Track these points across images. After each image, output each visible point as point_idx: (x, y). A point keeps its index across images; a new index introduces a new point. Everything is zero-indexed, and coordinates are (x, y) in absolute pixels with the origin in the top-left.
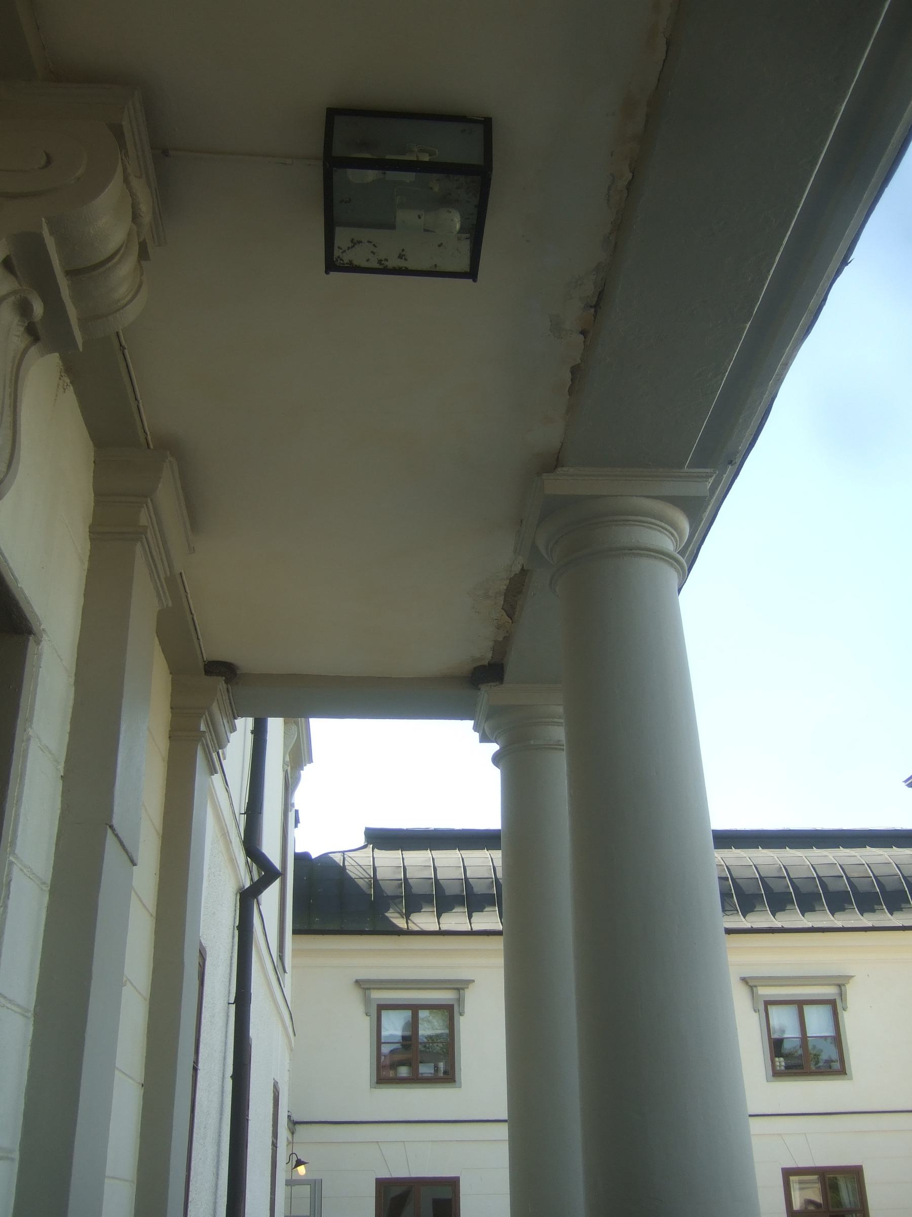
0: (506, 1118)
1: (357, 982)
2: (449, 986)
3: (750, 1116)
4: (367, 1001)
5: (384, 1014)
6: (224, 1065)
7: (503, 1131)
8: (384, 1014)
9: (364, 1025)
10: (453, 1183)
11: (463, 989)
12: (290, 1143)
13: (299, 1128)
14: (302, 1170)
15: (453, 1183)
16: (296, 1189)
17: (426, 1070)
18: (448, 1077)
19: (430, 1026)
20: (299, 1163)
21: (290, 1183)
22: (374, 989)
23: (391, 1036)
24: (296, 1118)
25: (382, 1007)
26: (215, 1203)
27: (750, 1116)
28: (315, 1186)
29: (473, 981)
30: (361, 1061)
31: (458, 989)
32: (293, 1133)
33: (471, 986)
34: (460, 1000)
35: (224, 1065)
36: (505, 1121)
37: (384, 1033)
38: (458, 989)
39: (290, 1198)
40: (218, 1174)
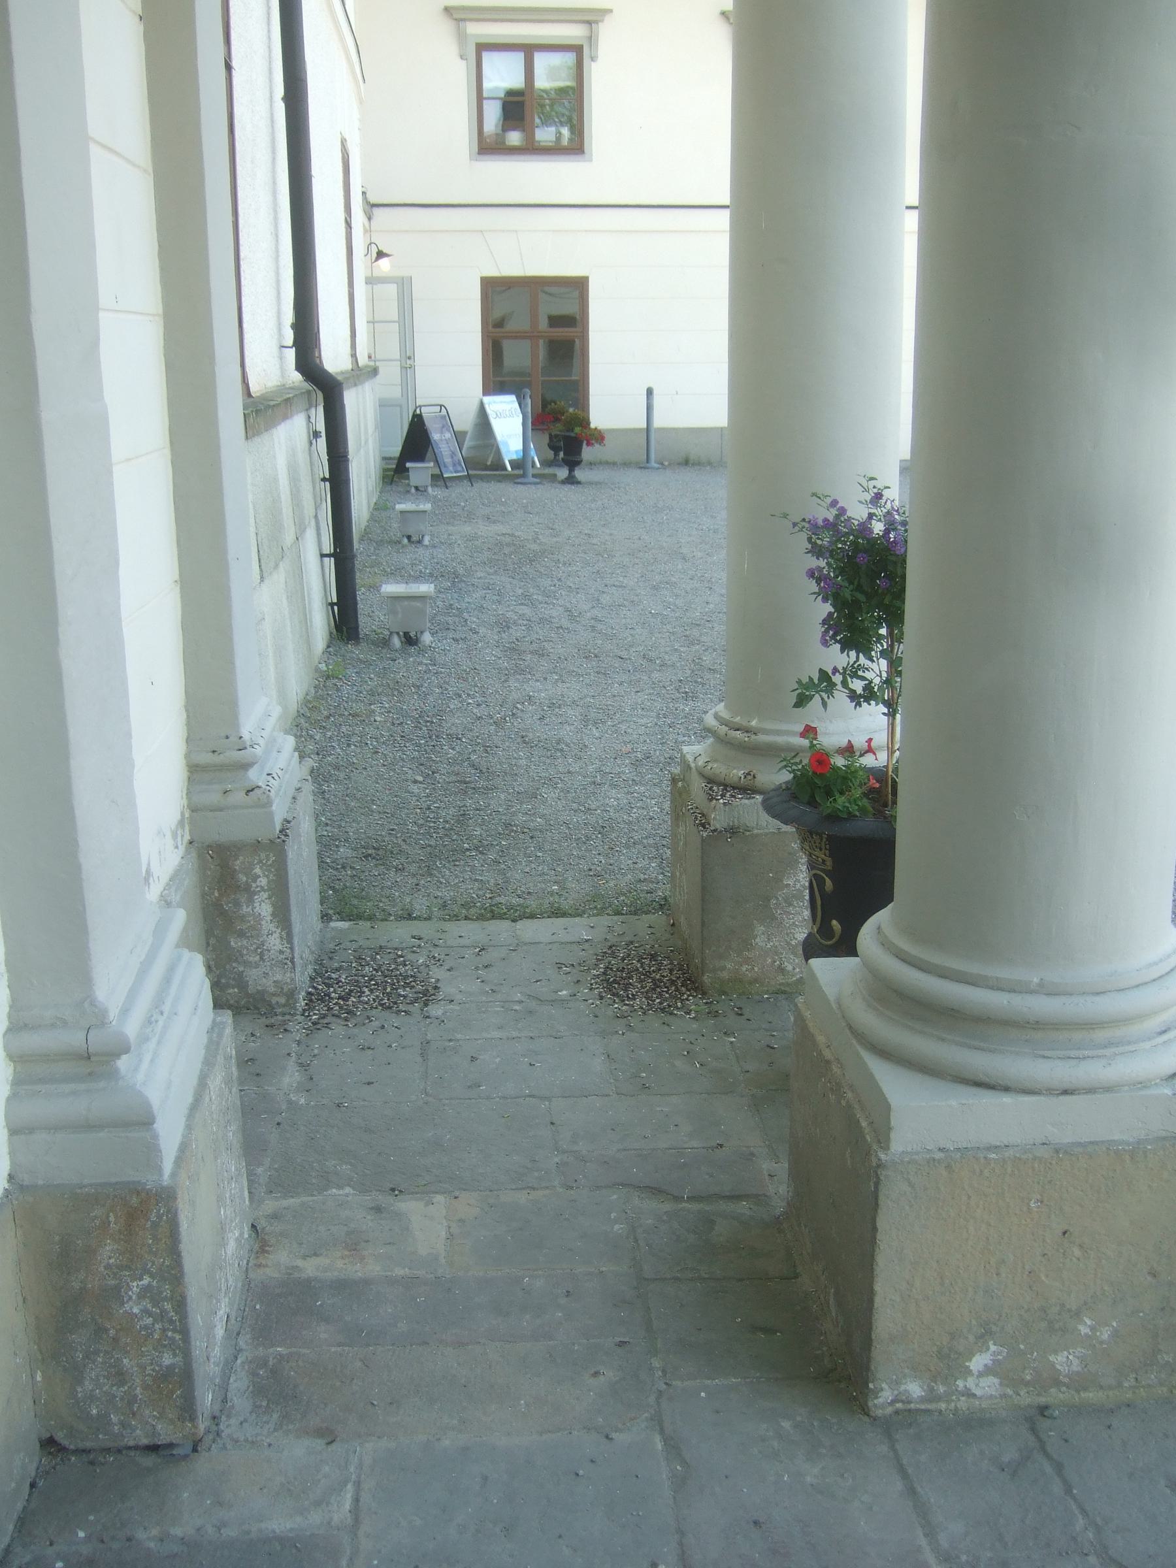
0: (727, 203)
1: (447, 10)
2: (580, 18)
3: (907, 208)
4: (462, 37)
5: (487, 57)
6: (269, 31)
7: (723, 220)
8: (487, 57)
9: (459, 73)
10: (579, 286)
11: (597, 22)
12: (368, 231)
13: (377, 212)
14: (384, 263)
15: (579, 286)
16: (378, 288)
17: (545, 135)
18: (576, 147)
19: (549, 73)
20: (381, 255)
21: (370, 281)
22: (471, 20)
23: (497, 88)
24: (373, 199)
25: (483, 48)
26: (277, 274)
27: (907, 208)
28: (404, 286)
29: (611, 11)
30: (453, 120)
31: (589, 23)
32: (369, 219)
33: (607, 18)
34: (591, 39)
35: (269, 31)
36: (727, 207)
37: (487, 85)
38: (589, 23)
39: (372, 301)
40: (277, 236)
